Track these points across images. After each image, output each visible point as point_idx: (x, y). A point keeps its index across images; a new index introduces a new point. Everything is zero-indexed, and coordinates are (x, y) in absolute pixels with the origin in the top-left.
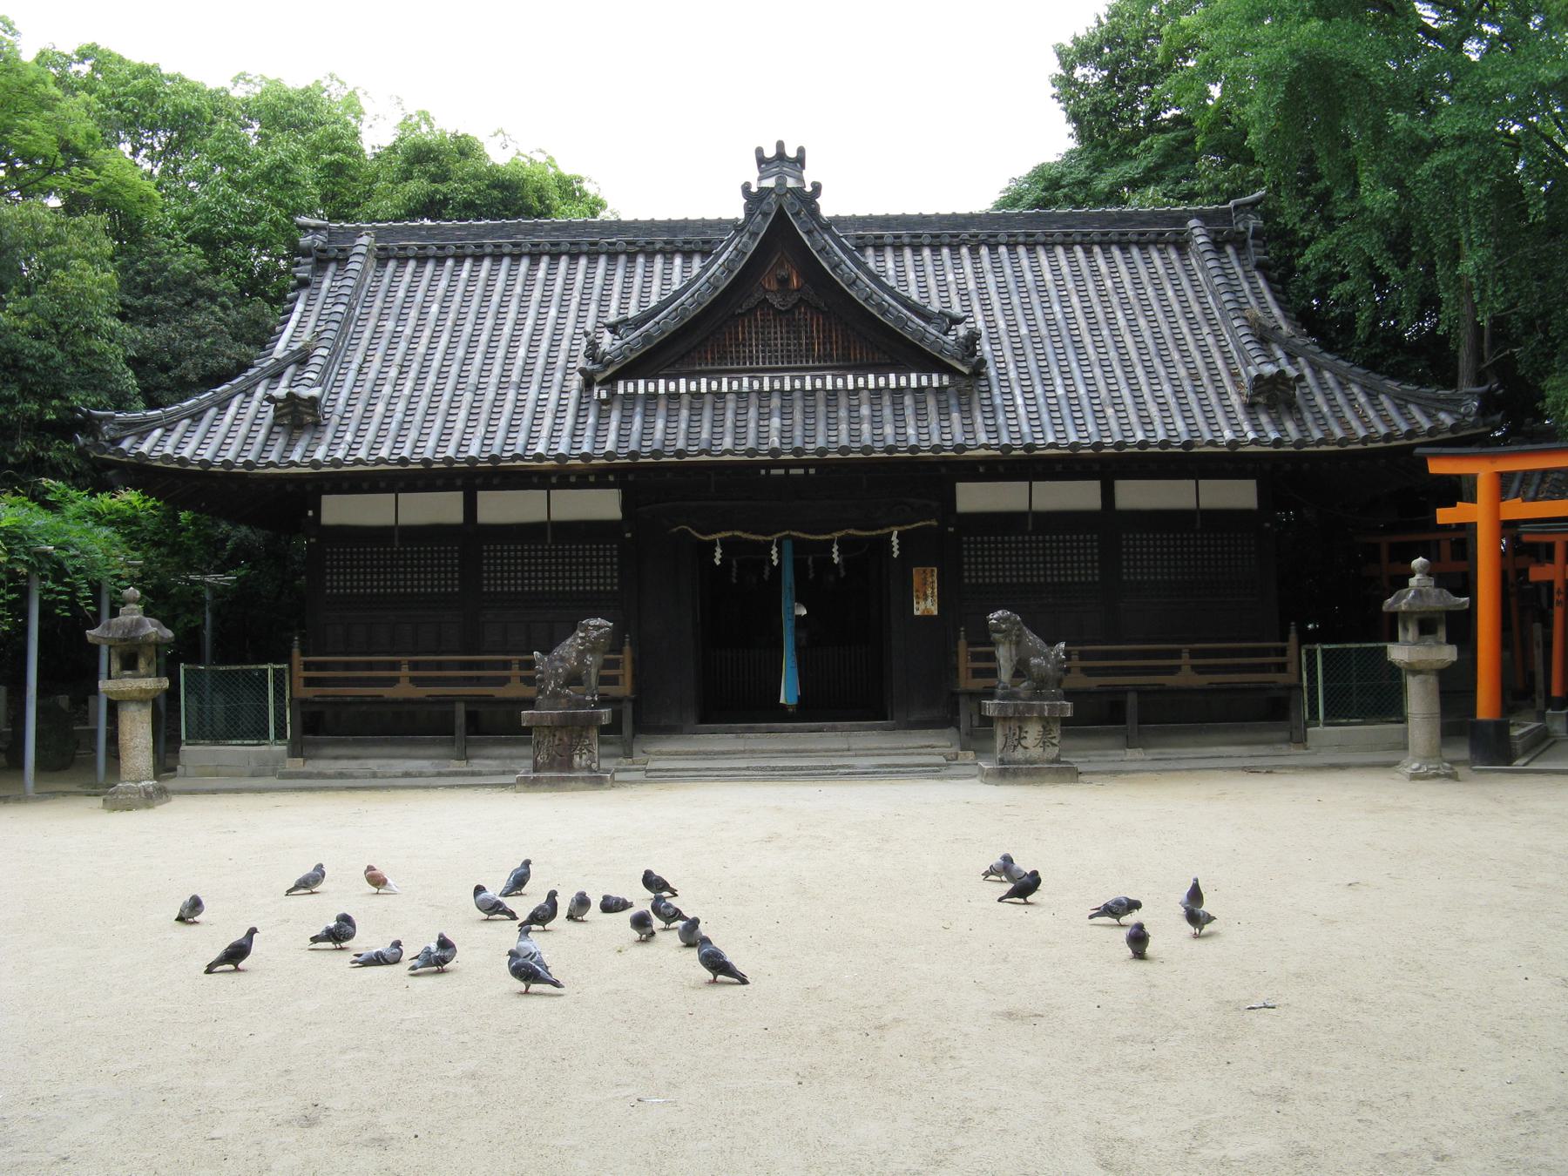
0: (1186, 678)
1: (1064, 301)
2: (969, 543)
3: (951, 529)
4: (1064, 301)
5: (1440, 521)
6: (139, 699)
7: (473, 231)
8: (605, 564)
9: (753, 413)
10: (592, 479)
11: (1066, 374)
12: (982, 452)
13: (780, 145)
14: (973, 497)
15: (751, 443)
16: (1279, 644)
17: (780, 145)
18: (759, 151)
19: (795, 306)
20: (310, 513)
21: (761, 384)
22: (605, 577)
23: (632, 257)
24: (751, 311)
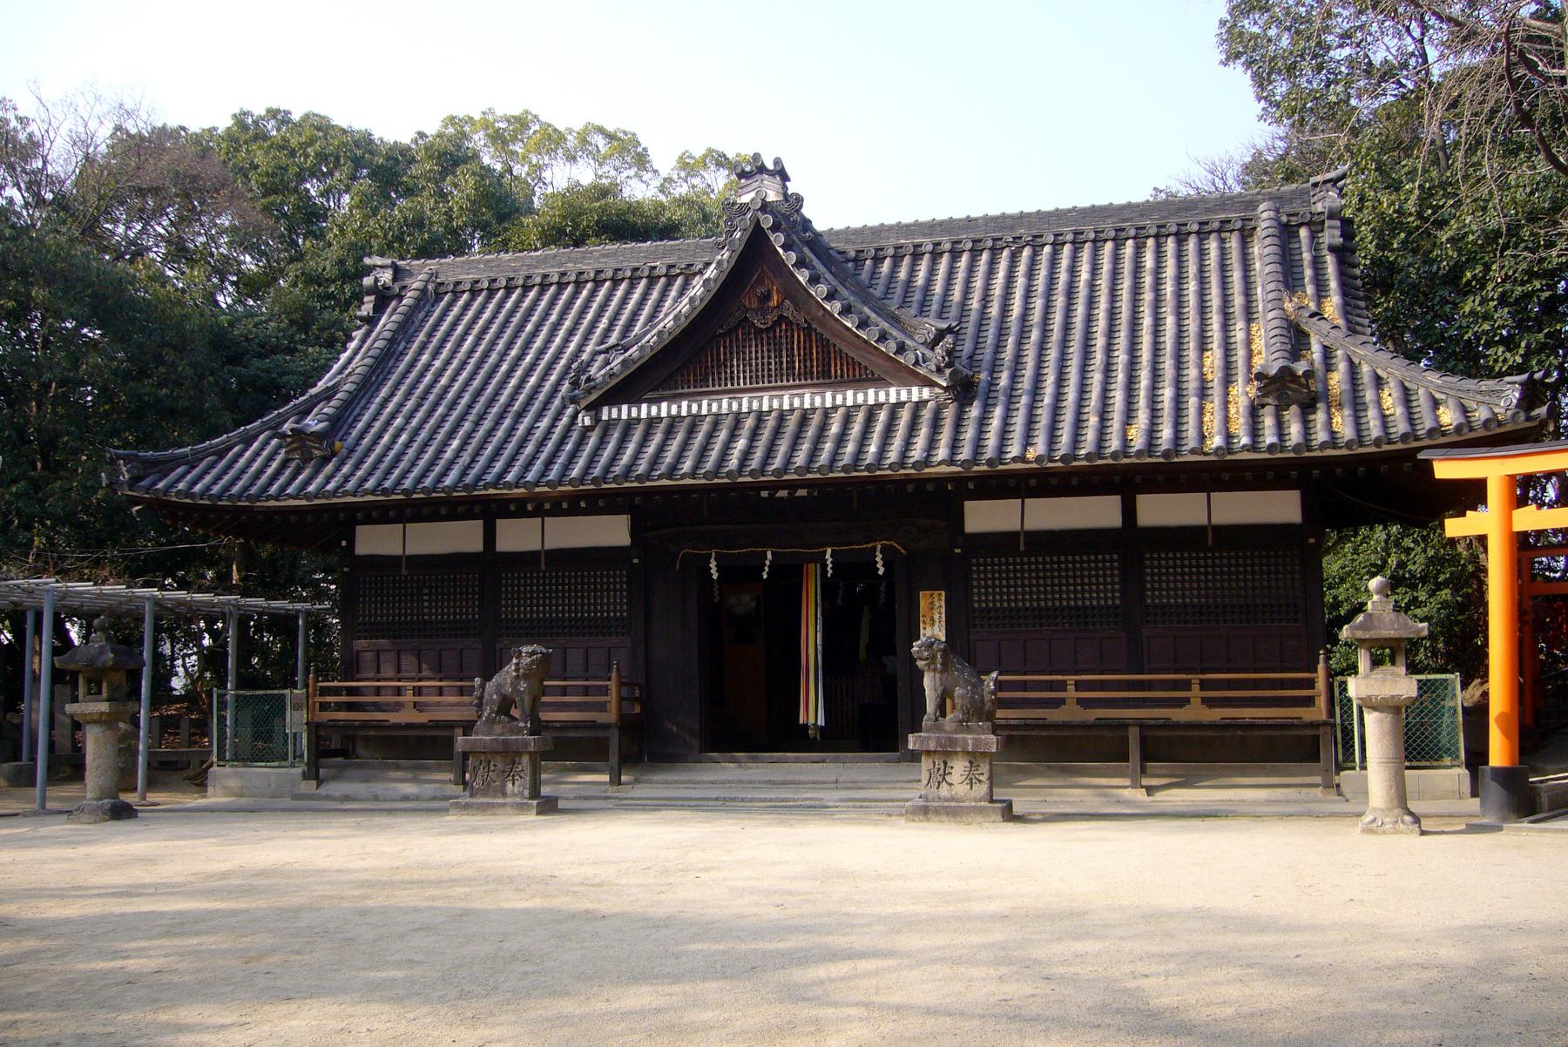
0: (1195, 712)
2: (978, 565)
3: (958, 551)
6: (99, 720)
7: (527, 262)
10: (565, 505)
14: (982, 517)
16: (1307, 675)
19: (775, 323)
20: (344, 543)
21: (740, 405)
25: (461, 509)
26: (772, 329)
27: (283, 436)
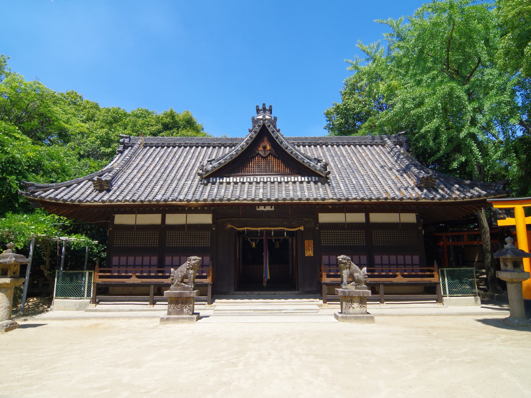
1: (351, 159)
3: (317, 228)
4: (351, 159)
8: (206, 238)
9: (254, 188)
11: (356, 178)
12: (331, 201)
13: (264, 105)
14: (324, 218)
15: (253, 197)
17: (264, 105)
18: (257, 107)
22: (206, 242)
23: (220, 147)
25: (147, 209)
26: (267, 157)
27: (94, 181)
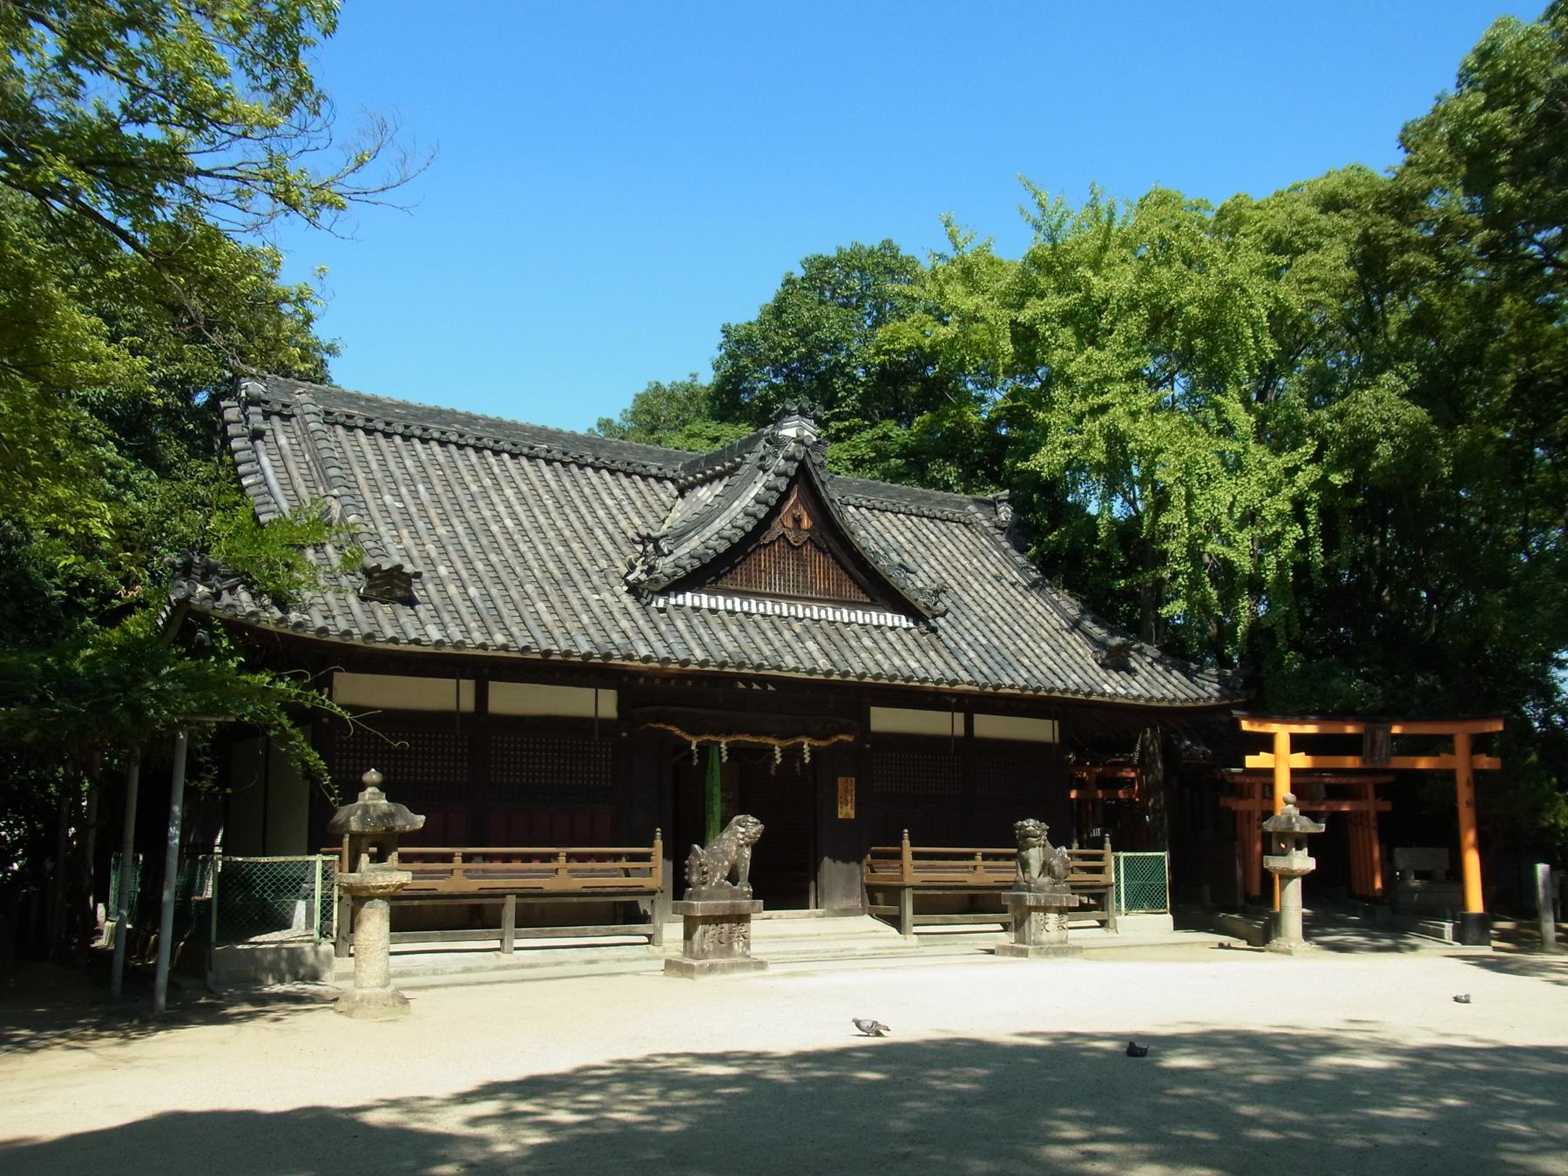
5: (1248, 765)
14: (884, 719)
24: (773, 542)
